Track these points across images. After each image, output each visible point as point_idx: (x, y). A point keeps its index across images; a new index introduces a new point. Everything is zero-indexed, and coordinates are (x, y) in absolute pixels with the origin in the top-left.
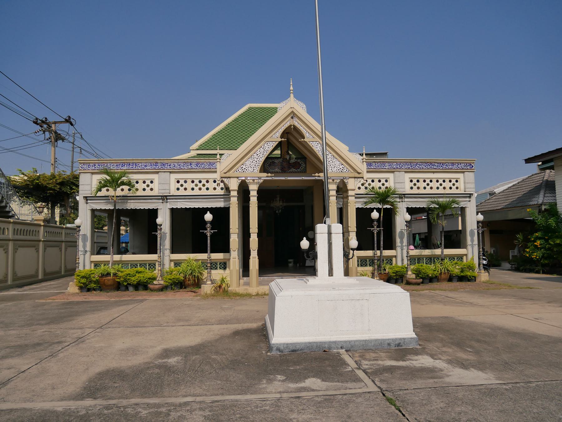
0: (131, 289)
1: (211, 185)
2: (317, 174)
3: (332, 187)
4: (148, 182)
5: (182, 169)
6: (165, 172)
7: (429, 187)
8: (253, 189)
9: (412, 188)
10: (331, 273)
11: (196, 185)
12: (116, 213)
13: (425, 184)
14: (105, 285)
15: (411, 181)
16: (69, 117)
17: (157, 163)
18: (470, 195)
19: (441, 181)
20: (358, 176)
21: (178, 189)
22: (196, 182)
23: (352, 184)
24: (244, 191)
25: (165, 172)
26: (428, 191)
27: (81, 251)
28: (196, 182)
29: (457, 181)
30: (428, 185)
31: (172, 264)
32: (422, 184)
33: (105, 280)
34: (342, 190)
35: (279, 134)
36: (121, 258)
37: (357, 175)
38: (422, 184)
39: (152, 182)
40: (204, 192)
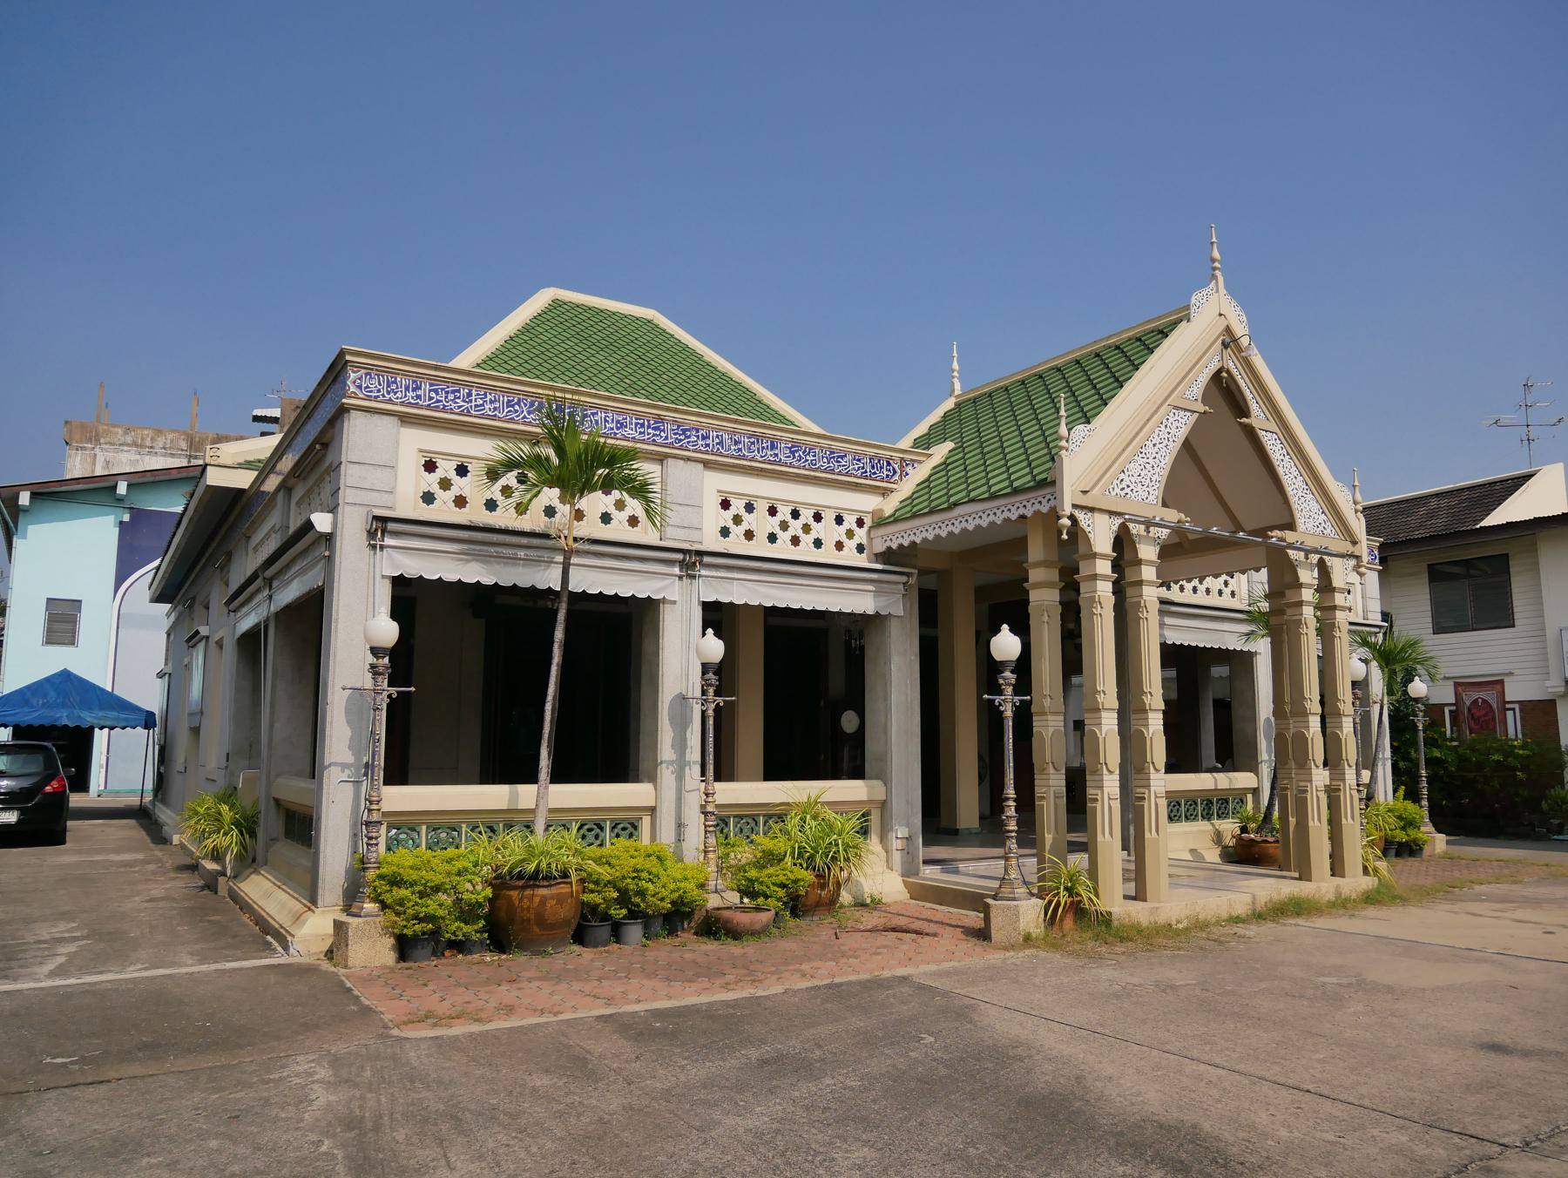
0: (635, 931)
1: (828, 531)
5: (744, 458)
6: (689, 459)
7: (449, 495)
12: (569, 603)
13: (773, 524)
17: (660, 419)
25: (689, 459)
27: (344, 766)
30: (445, 484)
33: (544, 900)
36: (514, 797)
38: (761, 523)
40: (806, 552)
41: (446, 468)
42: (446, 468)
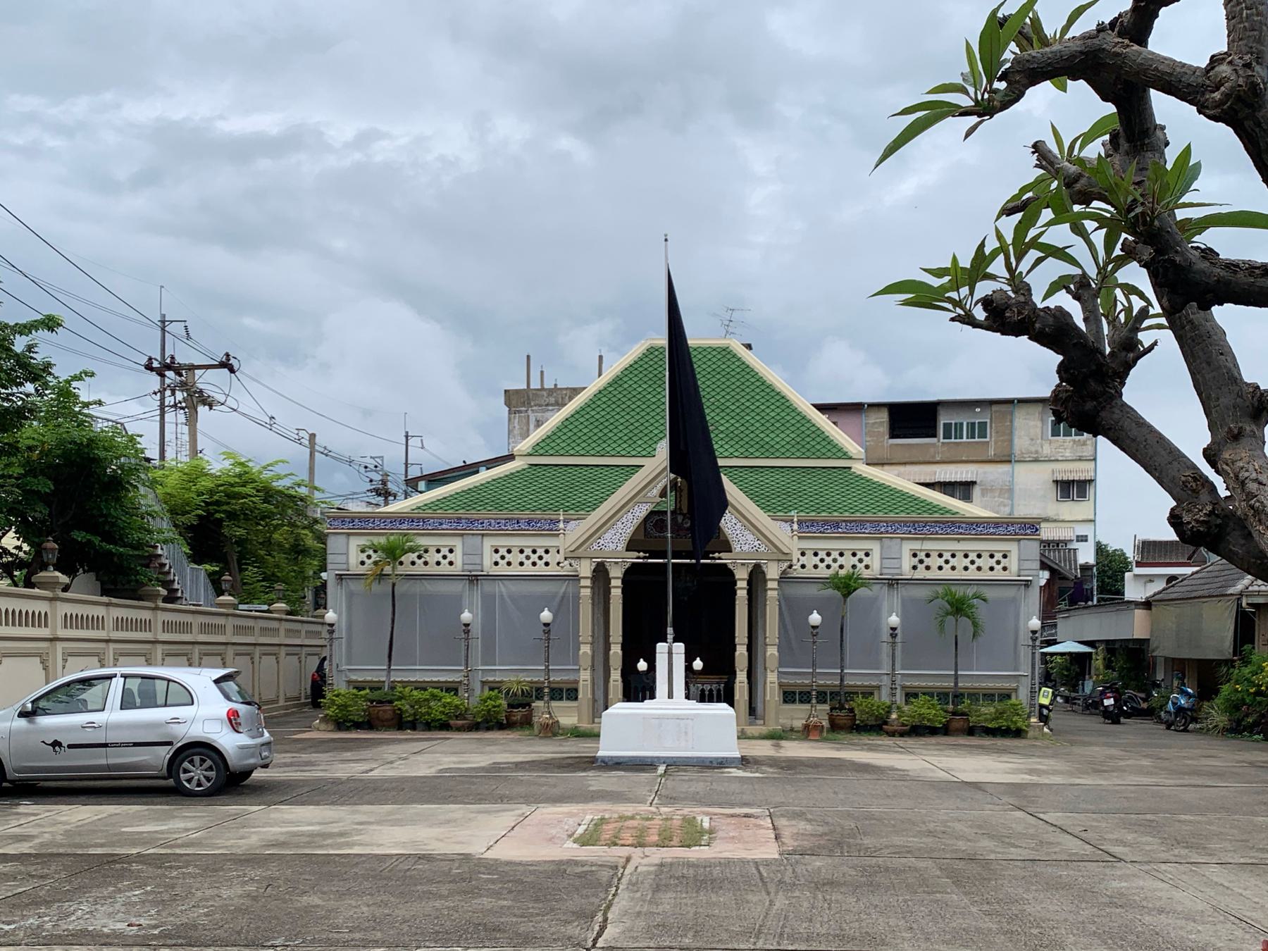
2: (716, 555)
3: (741, 575)
4: (445, 551)
7: (949, 566)
8: (616, 574)
9: (915, 568)
10: (670, 696)
11: (528, 558)
14: (378, 718)
15: (915, 555)
16: (227, 355)
17: (460, 519)
18: (1027, 584)
19: (947, 556)
20: (783, 556)
21: (496, 564)
22: (528, 552)
23: (773, 571)
24: (600, 573)
26: (947, 573)
28: (528, 552)
29: (1005, 556)
31: (486, 689)
32: (935, 561)
34: (757, 576)
35: (656, 491)
37: (784, 558)
38: (935, 561)
39: (451, 551)
40: (541, 569)
41: (503, 551)
42: (503, 551)
